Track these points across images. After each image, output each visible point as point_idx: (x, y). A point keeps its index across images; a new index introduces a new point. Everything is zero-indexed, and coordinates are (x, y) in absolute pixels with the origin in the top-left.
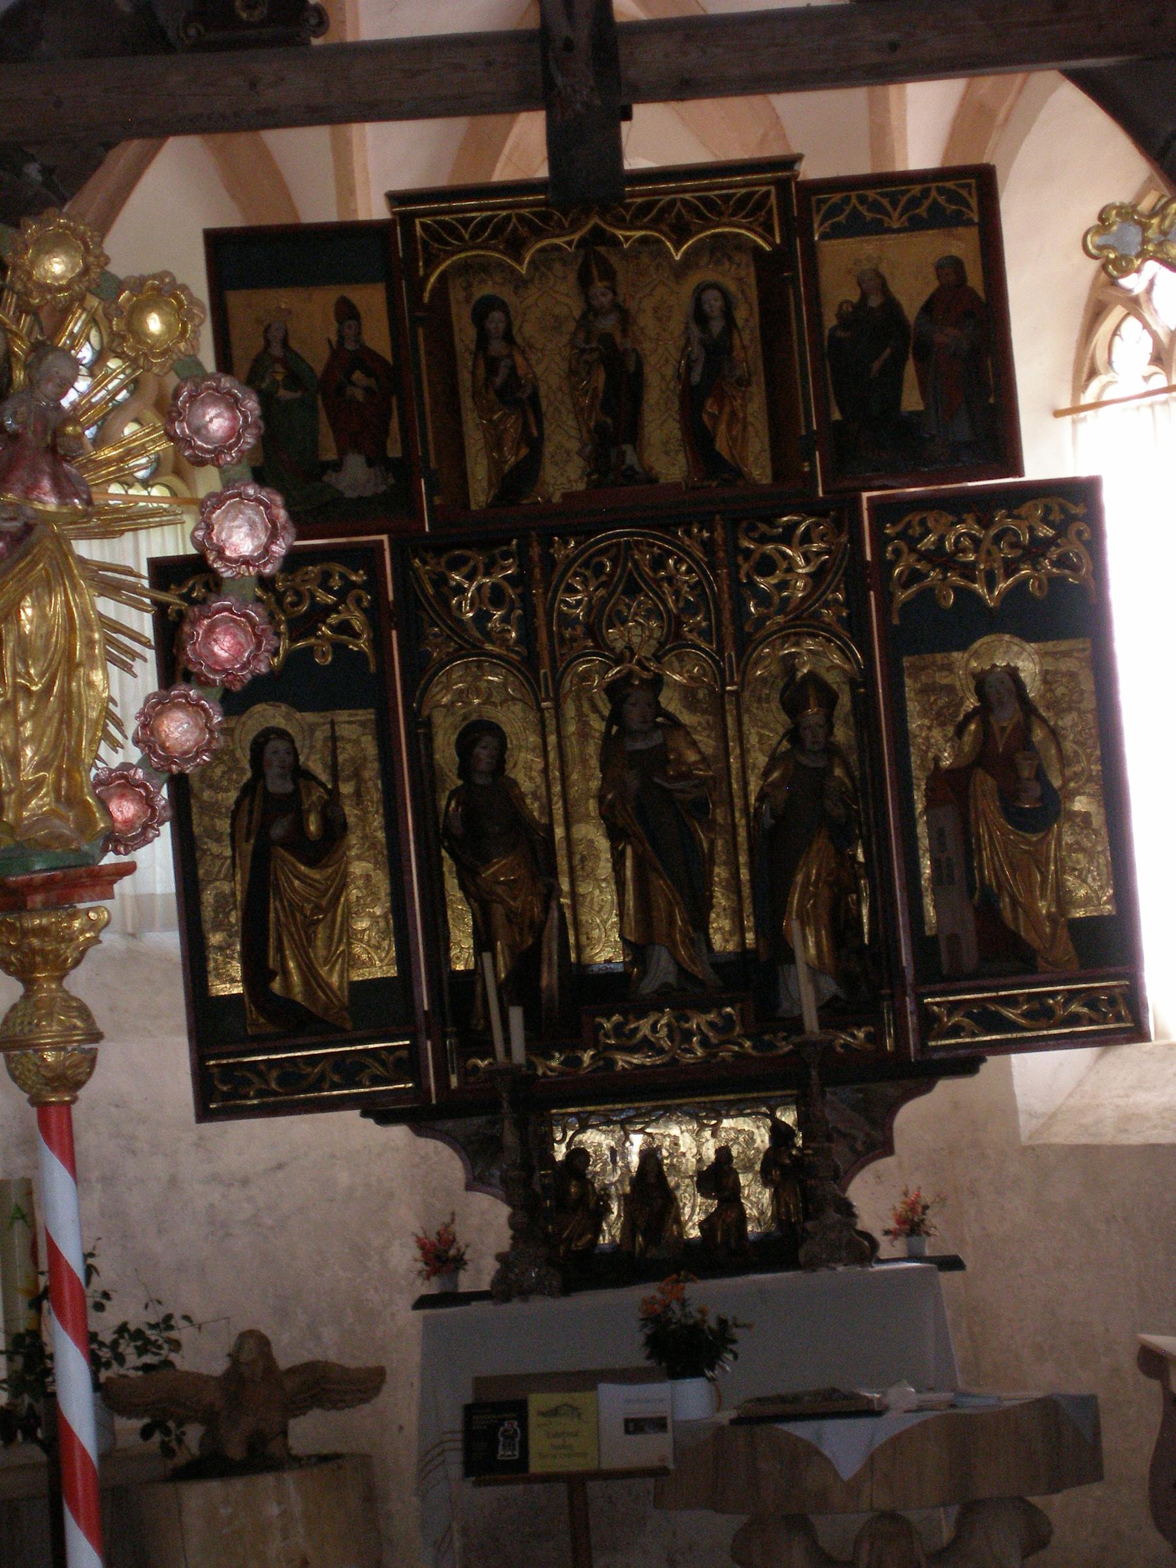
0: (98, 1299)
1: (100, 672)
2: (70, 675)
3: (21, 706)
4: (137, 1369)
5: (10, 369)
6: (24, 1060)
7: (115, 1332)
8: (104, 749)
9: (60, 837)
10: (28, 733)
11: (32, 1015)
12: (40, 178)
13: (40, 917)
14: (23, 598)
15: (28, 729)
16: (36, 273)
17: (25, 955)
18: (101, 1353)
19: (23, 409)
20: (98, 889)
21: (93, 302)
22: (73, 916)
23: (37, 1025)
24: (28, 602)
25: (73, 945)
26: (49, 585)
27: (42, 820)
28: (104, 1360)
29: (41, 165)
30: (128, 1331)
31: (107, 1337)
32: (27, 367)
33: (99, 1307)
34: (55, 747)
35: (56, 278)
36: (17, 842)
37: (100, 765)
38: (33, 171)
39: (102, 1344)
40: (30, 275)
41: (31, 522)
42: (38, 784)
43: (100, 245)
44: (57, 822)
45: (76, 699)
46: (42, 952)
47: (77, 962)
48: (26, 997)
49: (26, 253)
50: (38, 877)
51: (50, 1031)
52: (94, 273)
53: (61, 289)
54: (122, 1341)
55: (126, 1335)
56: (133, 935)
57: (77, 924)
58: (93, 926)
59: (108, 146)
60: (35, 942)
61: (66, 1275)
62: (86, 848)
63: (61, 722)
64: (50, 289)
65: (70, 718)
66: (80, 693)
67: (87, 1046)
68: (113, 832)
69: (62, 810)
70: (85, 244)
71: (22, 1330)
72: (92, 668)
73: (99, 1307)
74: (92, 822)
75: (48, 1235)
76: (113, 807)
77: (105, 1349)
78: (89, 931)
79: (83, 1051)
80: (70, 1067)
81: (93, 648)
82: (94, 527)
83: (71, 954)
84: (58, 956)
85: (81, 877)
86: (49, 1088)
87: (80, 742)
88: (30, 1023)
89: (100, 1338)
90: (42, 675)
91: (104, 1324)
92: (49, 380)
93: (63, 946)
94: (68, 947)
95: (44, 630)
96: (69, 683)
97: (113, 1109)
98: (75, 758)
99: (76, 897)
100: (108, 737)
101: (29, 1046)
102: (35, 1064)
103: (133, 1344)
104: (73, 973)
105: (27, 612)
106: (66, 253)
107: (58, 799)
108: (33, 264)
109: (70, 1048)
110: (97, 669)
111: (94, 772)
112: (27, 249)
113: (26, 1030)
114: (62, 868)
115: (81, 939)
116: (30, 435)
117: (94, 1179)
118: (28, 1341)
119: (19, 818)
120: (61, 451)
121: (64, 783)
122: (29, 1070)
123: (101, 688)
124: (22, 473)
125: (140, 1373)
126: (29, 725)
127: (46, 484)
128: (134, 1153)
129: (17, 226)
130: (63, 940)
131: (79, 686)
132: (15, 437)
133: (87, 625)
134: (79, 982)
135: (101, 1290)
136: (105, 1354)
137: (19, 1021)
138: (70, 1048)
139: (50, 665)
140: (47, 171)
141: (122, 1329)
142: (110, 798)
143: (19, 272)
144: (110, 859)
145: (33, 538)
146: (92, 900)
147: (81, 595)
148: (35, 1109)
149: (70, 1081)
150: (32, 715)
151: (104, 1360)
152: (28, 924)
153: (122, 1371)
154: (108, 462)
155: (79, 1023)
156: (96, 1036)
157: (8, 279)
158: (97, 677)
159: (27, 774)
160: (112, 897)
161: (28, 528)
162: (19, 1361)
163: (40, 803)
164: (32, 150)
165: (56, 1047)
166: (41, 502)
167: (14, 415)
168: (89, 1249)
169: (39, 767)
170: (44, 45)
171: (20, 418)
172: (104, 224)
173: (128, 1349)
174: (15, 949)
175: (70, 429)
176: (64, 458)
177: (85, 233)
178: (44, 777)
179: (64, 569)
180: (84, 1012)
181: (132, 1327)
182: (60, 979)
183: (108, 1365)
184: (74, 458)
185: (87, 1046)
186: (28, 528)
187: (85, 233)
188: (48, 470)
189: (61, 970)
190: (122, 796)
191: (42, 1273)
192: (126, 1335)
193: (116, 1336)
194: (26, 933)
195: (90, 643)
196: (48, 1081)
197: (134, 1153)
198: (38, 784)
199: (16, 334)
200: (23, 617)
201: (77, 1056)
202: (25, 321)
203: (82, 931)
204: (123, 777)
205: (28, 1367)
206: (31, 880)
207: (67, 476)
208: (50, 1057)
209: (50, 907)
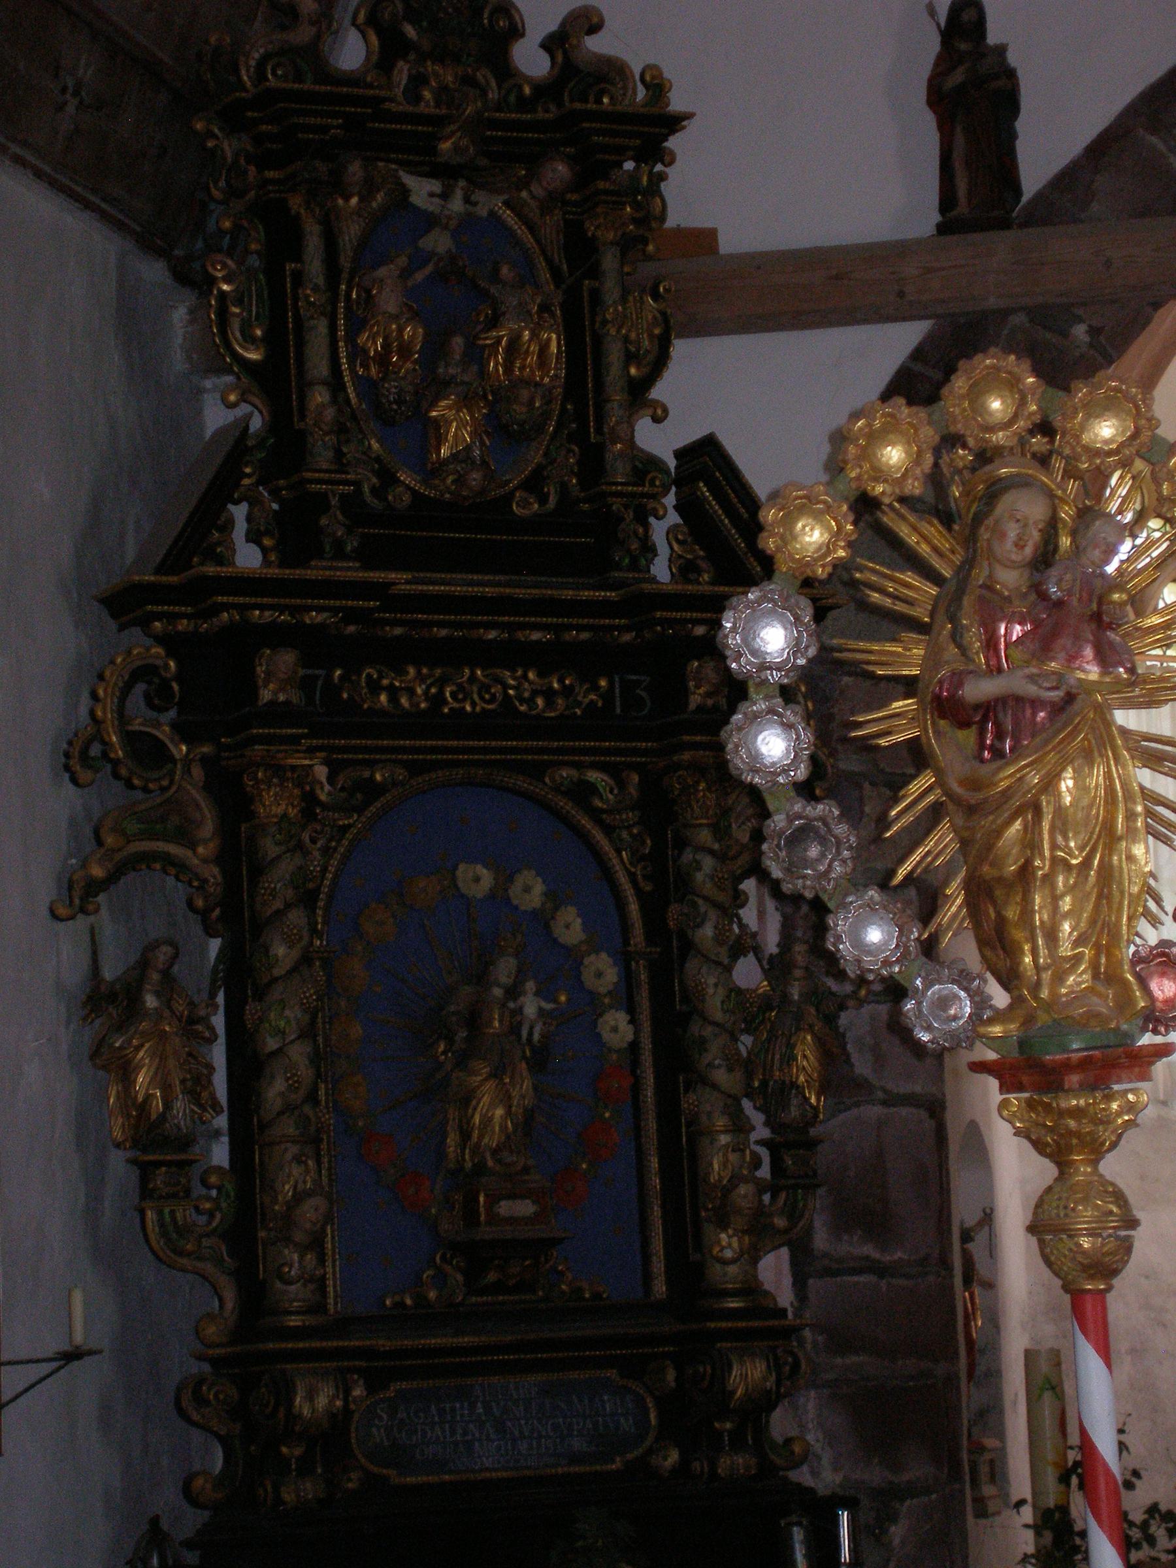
0: (1128, 1477)
1: (1142, 846)
2: (1110, 848)
3: (1060, 879)
4: (1168, 1552)
5: (1056, 535)
6: (1060, 1246)
7: (1146, 1512)
8: (1143, 926)
9: (1098, 1015)
10: (1067, 908)
11: (1068, 1199)
12: (1087, 339)
13: (1077, 1097)
14: (1064, 769)
15: (1066, 904)
16: (1086, 438)
17: (1061, 1136)
18: (1131, 1533)
19: (1068, 577)
20: (1137, 1070)
21: (1139, 465)
22: (1109, 1098)
23: (1073, 1209)
24: (1069, 773)
25: (1111, 1127)
26: (1088, 756)
27: (1079, 997)
28: (1134, 1540)
29: (1090, 326)
30: (1159, 1511)
31: (1137, 1517)
32: (1074, 534)
33: (1129, 1485)
34: (1093, 922)
35: (1106, 442)
36: (1055, 1020)
37: (1138, 941)
38: (1080, 331)
39: (1131, 1524)
40: (1078, 438)
41: (1074, 691)
42: (1077, 959)
43: (1149, 407)
44: (1095, 999)
45: (1117, 874)
46: (1078, 1134)
47: (1114, 1145)
48: (1062, 1176)
49: (1075, 418)
50: (1075, 1056)
51: (1085, 1216)
52: (1145, 436)
53: (1110, 453)
54: (1152, 1522)
55: (1157, 1516)
56: (1164, 1103)
57: (1115, 1106)
58: (1131, 1108)
59: (1157, 306)
60: (1072, 1123)
61: (1100, 1469)
62: (1125, 1027)
63: (1100, 896)
64: (1098, 453)
65: (1110, 893)
66: (1121, 868)
67: (1123, 1233)
68: (1153, 1011)
69: (1100, 988)
70: (1137, 407)
71: (1052, 1505)
72: (1134, 841)
73: (1129, 1485)
74: (1131, 1001)
75: (1083, 1433)
76: (1154, 986)
77: (1134, 1529)
78: (1128, 1113)
79: (1118, 1238)
80: (1107, 1254)
81: (1135, 821)
82: (1138, 697)
83: (1108, 1137)
84: (1094, 1140)
85: (1119, 1057)
86: (1084, 1275)
87: (1119, 918)
88: (1065, 1207)
89: (1130, 1517)
90: (1081, 849)
91: (1136, 1503)
92: (1096, 547)
93: (1101, 1128)
94: (1105, 1131)
95: (1085, 802)
96: (1110, 855)
97: (1143, 1279)
98: (1115, 936)
99: (1114, 1078)
100: (1147, 913)
101: (1064, 1231)
102: (1070, 1250)
103: (1164, 1525)
104: (1109, 1156)
105: (1067, 783)
106: (1117, 416)
107: (1096, 976)
108: (1083, 427)
109: (1105, 1235)
110: (1139, 842)
111: (1132, 949)
112: (1076, 412)
113: (1062, 1215)
114: (1101, 1047)
115: (1120, 1121)
116: (1075, 602)
117: (1123, 1351)
118: (1057, 1515)
119: (1054, 994)
120: (1106, 619)
121: (1103, 960)
122: (1065, 1256)
123: (1143, 863)
124: (1065, 641)
125: (1171, 1557)
126: (1068, 899)
127: (1089, 652)
128: (1164, 1325)
129: (1067, 389)
130: (1101, 1122)
131: (1120, 860)
132: (1060, 604)
133: (1129, 797)
134: (1112, 1167)
135: (1131, 1468)
136: (1135, 1534)
137: (1054, 1204)
138: (1105, 1235)
139: (1090, 839)
140: (1094, 331)
141: (1153, 1510)
142: (1151, 975)
143: (1068, 437)
144: (1147, 1039)
145: (1076, 707)
146: (1131, 1081)
147: (1124, 767)
148: (1069, 1296)
149: (1106, 1268)
150: (1070, 890)
151: (1134, 1540)
152: (1064, 1104)
153: (1153, 1554)
154: (1153, 629)
155: (1115, 1210)
156: (1133, 1223)
157: (1057, 443)
158: (1138, 850)
159: (1065, 950)
160: (1150, 1079)
161: (1070, 698)
162: (1048, 1537)
163: (1078, 980)
164: (1080, 312)
165: (1092, 1233)
166: (1084, 671)
167: (1058, 583)
168: (1120, 1426)
169: (1077, 943)
170: (1095, 207)
171: (1065, 586)
172: (1149, 381)
173: (1159, 1531)
174: (1051, 1130)
175: (1116, 596)
176: (1110, 627)
177: (1136, 395)
178: (1082, 953)
179: (1104, 740)
180: (1119, 1197)
181: (1163, 1508)
182: (1095, 1163)
183: (1138, 1546)
184: (1119, 626)
185: (1123, 1233)
186: (1070, 698)
187: (1136, 395)
188: (1091, 638)
189: (1097, 1151)
190: (1163, 974)
191: (1071, 1448)
192: (1157, 1516)
193: (1146, 1516)
194: (1063, 1113)
195: (1131, 816)
196: (1085, 1268)
197: (1164, 1325)
198: (1077, 959)
199: (1061, 499)
200: (1063, 787)
201: (1111, 1245)
202: (1072, 486)
203: (1119, 1114)
204: (1163, 954)
205: (1058, 1542)
206: (1069, 1059)
207: (1111, 644)
208: (1086, 1243)
209: (1091, 1087)
